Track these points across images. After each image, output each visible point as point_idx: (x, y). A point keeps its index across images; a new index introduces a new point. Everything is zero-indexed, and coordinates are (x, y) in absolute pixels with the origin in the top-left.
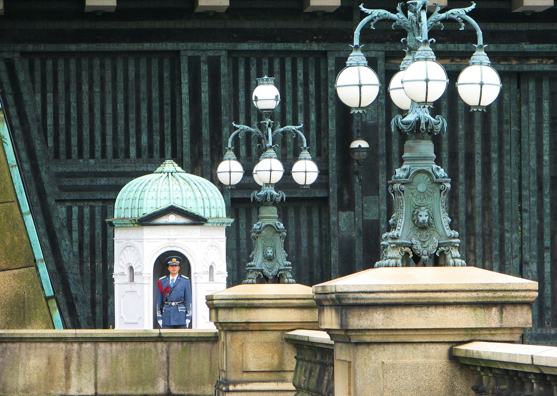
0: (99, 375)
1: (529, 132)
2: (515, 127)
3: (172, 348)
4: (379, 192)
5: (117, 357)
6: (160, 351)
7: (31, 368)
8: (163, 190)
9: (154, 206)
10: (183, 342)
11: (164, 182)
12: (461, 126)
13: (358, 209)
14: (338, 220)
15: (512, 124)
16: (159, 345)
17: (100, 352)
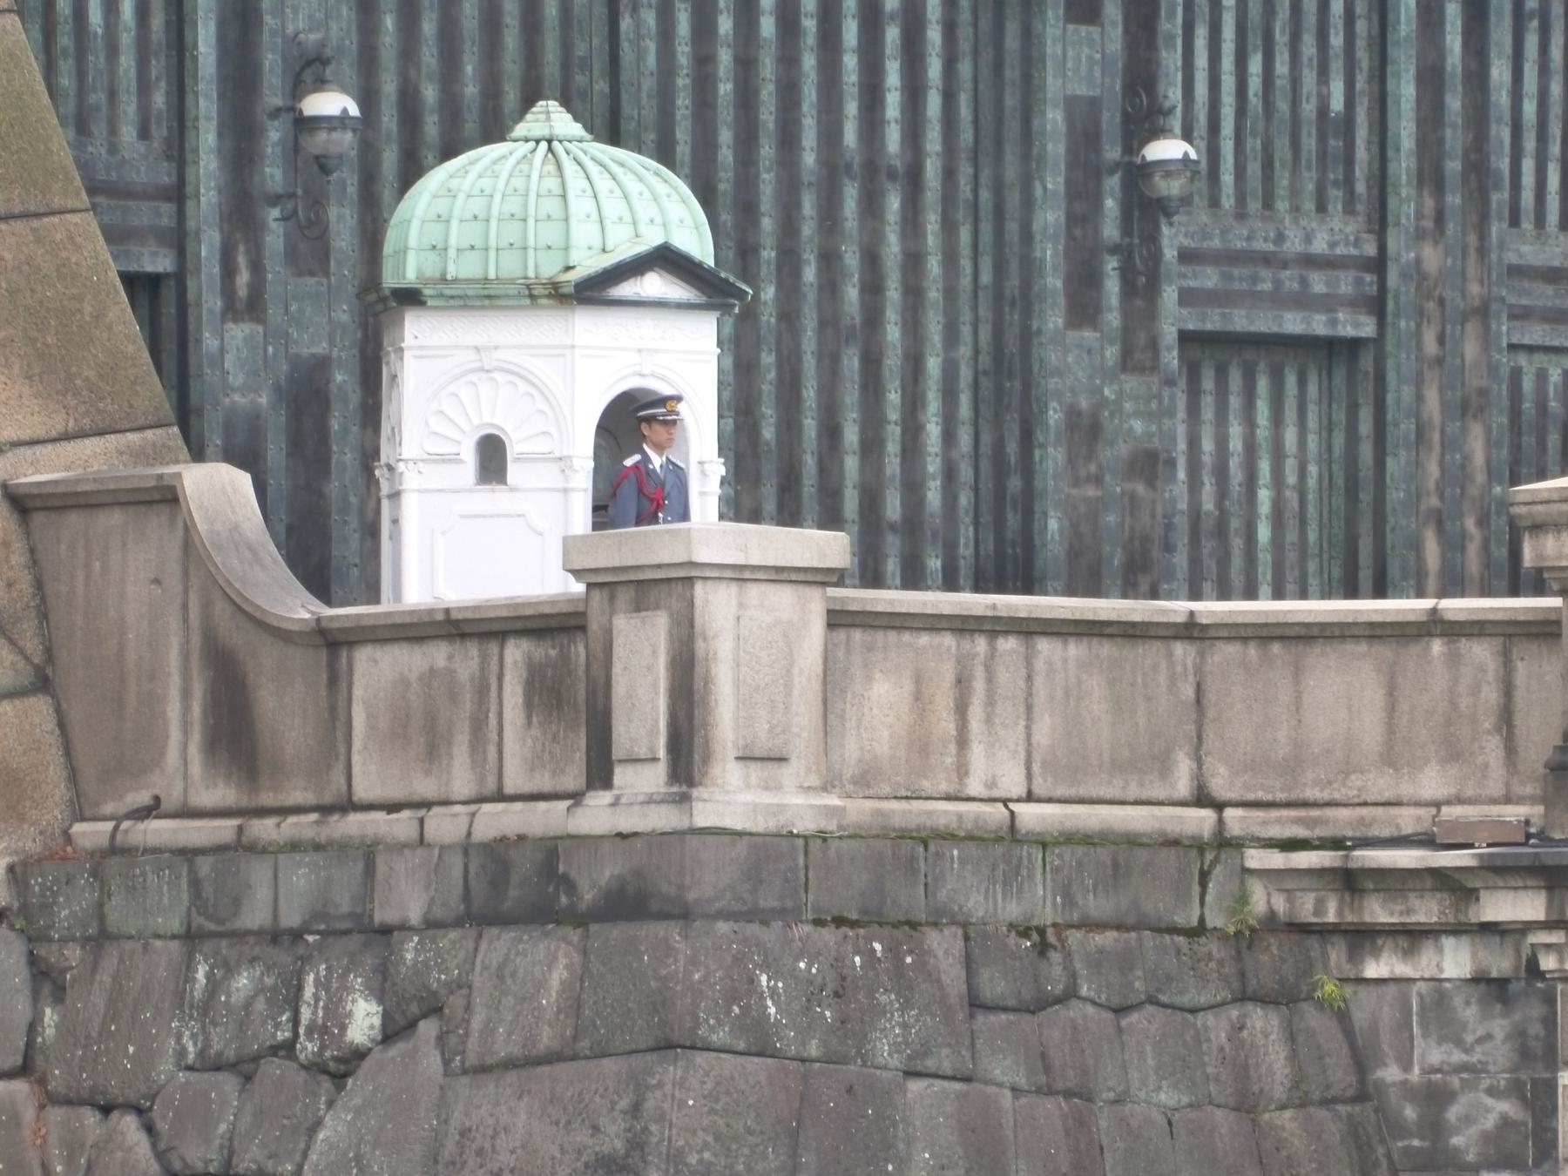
0: (1036, 738)
1: (639, 102)
2: (602, 83)
3: (1217, 658)
4: (328, 266)
5: (1079, 683)
6: (1179, 668)
7: (876, 711)
10: (1245, 640)
12: (469, 69)
13: (274, 312)
14: (222, 350)
15: (596, 73)
16: (1179, 648)
17: (1039, 665)
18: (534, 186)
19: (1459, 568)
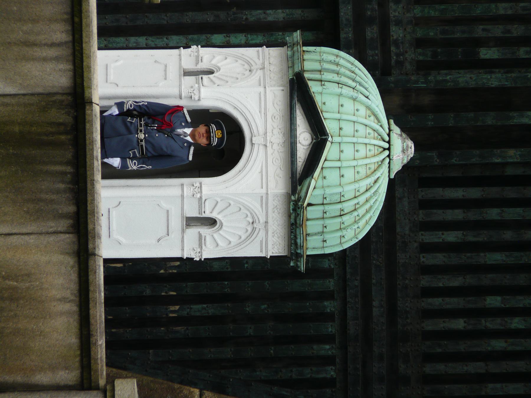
8: (357, 169)
9: (324, 108)
11: (372, 148)
18: (361, 162)
19: (35, 99)
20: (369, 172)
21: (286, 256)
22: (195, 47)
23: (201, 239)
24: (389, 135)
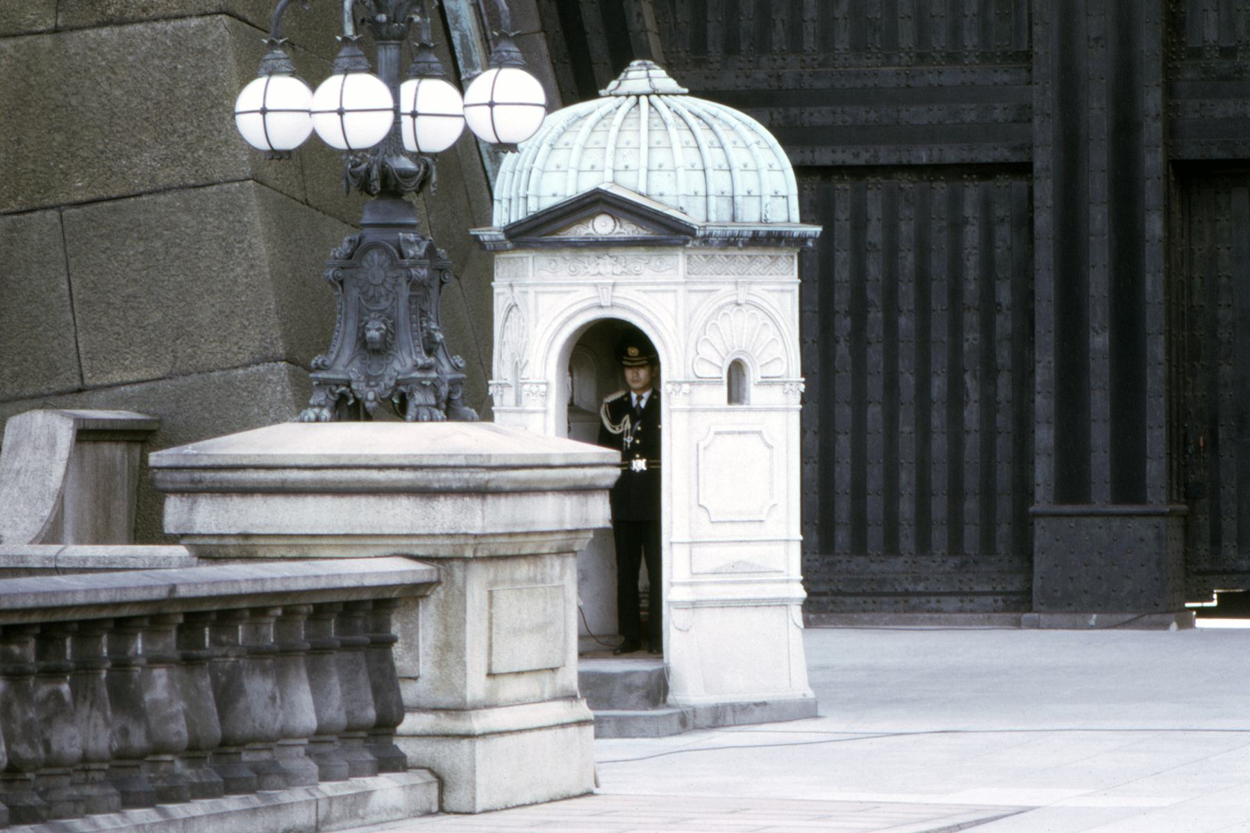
20: (663, 127)
21: (800, 255)
22: (491, 389)
23: (767, 382)
24: (628, 96)
